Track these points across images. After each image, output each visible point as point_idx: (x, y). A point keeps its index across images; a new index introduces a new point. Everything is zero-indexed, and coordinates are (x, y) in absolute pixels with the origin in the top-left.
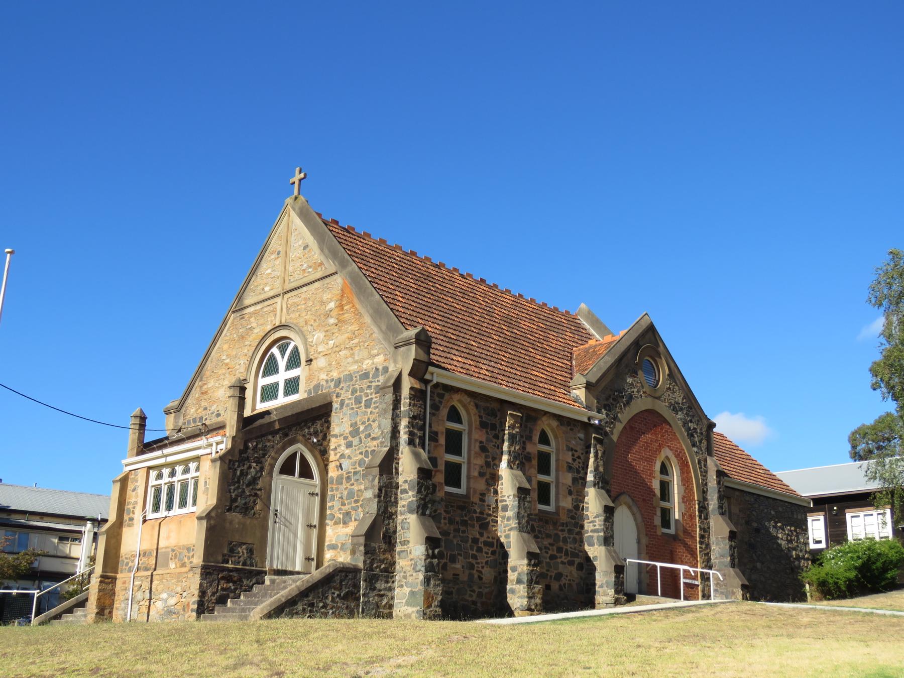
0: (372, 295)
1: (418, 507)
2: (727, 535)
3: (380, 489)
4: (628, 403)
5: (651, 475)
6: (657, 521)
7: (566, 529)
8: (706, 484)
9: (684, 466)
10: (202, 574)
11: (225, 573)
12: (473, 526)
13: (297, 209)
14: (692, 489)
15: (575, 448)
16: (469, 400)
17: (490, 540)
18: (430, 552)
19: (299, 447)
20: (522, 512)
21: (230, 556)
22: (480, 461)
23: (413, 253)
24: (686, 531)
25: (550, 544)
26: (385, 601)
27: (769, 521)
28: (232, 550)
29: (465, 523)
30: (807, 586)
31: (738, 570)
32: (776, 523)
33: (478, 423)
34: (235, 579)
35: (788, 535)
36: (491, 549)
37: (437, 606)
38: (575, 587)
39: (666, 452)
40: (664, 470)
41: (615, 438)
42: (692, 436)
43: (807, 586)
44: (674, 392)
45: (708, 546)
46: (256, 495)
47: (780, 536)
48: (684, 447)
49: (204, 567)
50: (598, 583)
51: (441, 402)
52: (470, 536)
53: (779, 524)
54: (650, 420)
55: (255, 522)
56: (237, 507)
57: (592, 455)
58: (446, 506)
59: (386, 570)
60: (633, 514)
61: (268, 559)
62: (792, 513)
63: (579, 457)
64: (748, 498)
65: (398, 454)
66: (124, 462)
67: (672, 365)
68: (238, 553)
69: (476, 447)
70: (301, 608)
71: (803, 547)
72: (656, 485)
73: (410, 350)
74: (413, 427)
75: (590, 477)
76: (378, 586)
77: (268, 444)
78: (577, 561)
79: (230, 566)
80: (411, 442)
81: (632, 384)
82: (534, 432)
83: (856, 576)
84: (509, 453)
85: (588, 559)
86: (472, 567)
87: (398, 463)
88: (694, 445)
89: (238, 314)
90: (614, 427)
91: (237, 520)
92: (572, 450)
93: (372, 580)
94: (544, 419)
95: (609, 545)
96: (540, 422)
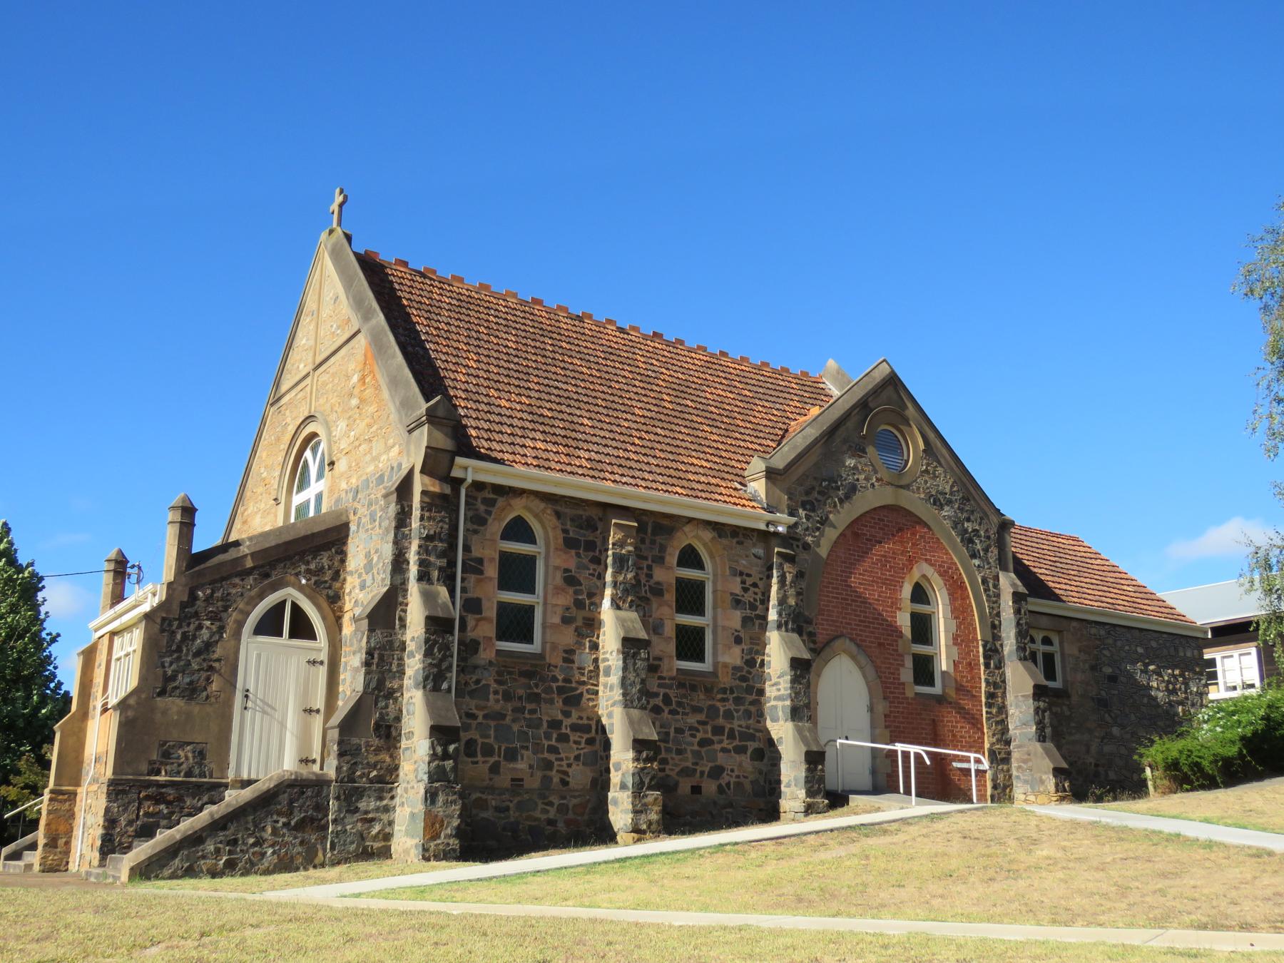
0: (394, 356)
1: (426, 679)
2: (1030, 691)
3: (370, 653)
4: (848, 497)
5: (895, 605)
6: (907, 674)
7: (731, 697)
8: (998, 615)
9: (956, 589)
10: (109, 794)
11: (151, 791)
12: (551, 702)
13: (329, 246)
14: (972, 624)
15: (746, 571)
16: (542, 505)
17: (585, 722)
18: (439, 749)
19: (290, 594)
20: (632, 676)
21: (162, 763)
22: (565, 600)
23: (536, 301)
24: (960, 689)
25: (699, 722)
26: (376, 829)
27: (1134, 663)
28: (166, 755)
29: (535, 698)
30: (1148, 771)
31: (1050, 745)
32: (1146, 665)
33: (561, 541)
34: (171, 798)
35: (1169, 682)
36: (586, 736)
37: (450, 836)
38: (748, 787)
39: (922, 570)
40: (920, 594)
41: (823, 551)
42: (971, 541)
43: (1148, 771)
44: (935, 477)
45: (1003, 709)
46: (211, 668)
47: (1155, 684)
48: (956, 560)
49: (112, 783)
50: (784, 779)
51: (489, 513)
52: (545, 718)
53: (1152, 667)
54: (893, 521)
55: (209, 709)
56: (176, 688)
57: (775, 580)
58: (499, 673)
59: (380, 780)
60: (861, 668)
61: (233, 764)
62: (1176, 650)
63: (755, 585)
64: (1093, 631)
65: (405, 596)
66: (92, 625)
67: (931, 436)
68: (179, 758)
69: (558, 579)
70: (212, 848)
71: (1197, 699)
72: (904, 621)
73: (422, 434)
74: (428, 552)
75: (773, 615)
76: (362, 805)
77: (233, 591)
78: (752, 746)
79: (162, 778)
80: (423, 577)
81: (855, 468)
82: (669, 550)
83: (1240, 751)
84: (615, 585)
85: (771, 742)
86: (548, 765)
87: (405, 611)
88: (974, 556)
89: (276, 407)
90: (822, 535)
91: (175, 709)
92: (741, 574)
93: (350, 797)
94: (687, 529)
95: (801, 719)
96: (679, 534)
